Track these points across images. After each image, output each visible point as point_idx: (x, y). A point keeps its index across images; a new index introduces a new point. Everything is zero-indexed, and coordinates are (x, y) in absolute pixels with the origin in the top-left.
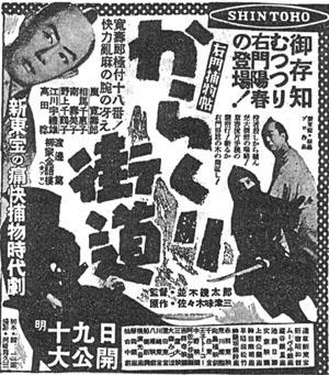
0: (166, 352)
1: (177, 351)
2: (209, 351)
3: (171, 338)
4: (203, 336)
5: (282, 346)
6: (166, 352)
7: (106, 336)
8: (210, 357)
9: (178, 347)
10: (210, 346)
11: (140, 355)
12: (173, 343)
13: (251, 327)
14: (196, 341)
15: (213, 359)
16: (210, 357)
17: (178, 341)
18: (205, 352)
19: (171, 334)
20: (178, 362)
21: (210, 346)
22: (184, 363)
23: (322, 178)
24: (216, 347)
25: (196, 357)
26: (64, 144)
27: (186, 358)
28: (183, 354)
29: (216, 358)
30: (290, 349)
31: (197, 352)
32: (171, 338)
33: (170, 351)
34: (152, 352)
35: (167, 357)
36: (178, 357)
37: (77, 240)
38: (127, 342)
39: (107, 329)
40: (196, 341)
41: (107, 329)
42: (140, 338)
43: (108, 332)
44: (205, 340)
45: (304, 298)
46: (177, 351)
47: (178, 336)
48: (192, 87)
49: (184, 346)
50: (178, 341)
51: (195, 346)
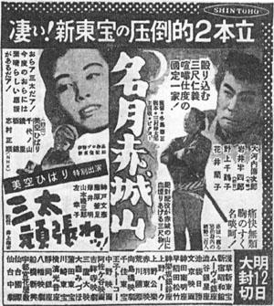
0: (71, 284)
1: (86, 283)
2: (124, 284)
3: (79, 269)
4: (117, 266)
5: (206, 278)
6: (71, 284)
7: (259, 295)
8: (125, 290)
9: (87, 278)
10: (125, 278)
11: (56, 287)
12: (81, 274)
13: (5, 140)
14: (109, 271)
15: (128, 292)
16: (125, 290)
17: (86, 272)
18: (119, 285)
19: (79, 263)
20: (86, 297)
21: (125, 278)
22: (93, 297)
23: (130, 6)
24: (132, 278)
25: (108, 290)
26: (12, 140)
27: (95, 292)
28: (93, 287)
29: (132, 292)
30: (214, 281)
31: (109, 284)
32: (79, 269)
33: (77, 283)
34: (40, 284)
35: (74, 291)
36: (87, 290)
37: (102, 231)
38: (229, 287)
39: (261, 295)
40: (109, 271)
41: (261, 295)
42: (56, 269)
43: (261, 293)
44: (119, 270)
45: (187, 126)
46: (86, 283)
47: (86, 265)
48: (184, 249)
49: (94, 278)
50: (86, 272)
51: (107, 278)
